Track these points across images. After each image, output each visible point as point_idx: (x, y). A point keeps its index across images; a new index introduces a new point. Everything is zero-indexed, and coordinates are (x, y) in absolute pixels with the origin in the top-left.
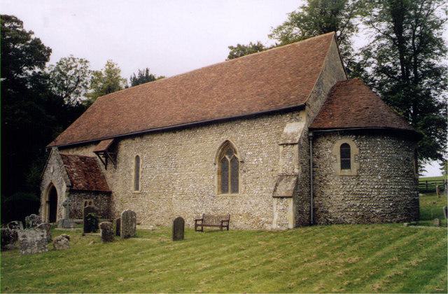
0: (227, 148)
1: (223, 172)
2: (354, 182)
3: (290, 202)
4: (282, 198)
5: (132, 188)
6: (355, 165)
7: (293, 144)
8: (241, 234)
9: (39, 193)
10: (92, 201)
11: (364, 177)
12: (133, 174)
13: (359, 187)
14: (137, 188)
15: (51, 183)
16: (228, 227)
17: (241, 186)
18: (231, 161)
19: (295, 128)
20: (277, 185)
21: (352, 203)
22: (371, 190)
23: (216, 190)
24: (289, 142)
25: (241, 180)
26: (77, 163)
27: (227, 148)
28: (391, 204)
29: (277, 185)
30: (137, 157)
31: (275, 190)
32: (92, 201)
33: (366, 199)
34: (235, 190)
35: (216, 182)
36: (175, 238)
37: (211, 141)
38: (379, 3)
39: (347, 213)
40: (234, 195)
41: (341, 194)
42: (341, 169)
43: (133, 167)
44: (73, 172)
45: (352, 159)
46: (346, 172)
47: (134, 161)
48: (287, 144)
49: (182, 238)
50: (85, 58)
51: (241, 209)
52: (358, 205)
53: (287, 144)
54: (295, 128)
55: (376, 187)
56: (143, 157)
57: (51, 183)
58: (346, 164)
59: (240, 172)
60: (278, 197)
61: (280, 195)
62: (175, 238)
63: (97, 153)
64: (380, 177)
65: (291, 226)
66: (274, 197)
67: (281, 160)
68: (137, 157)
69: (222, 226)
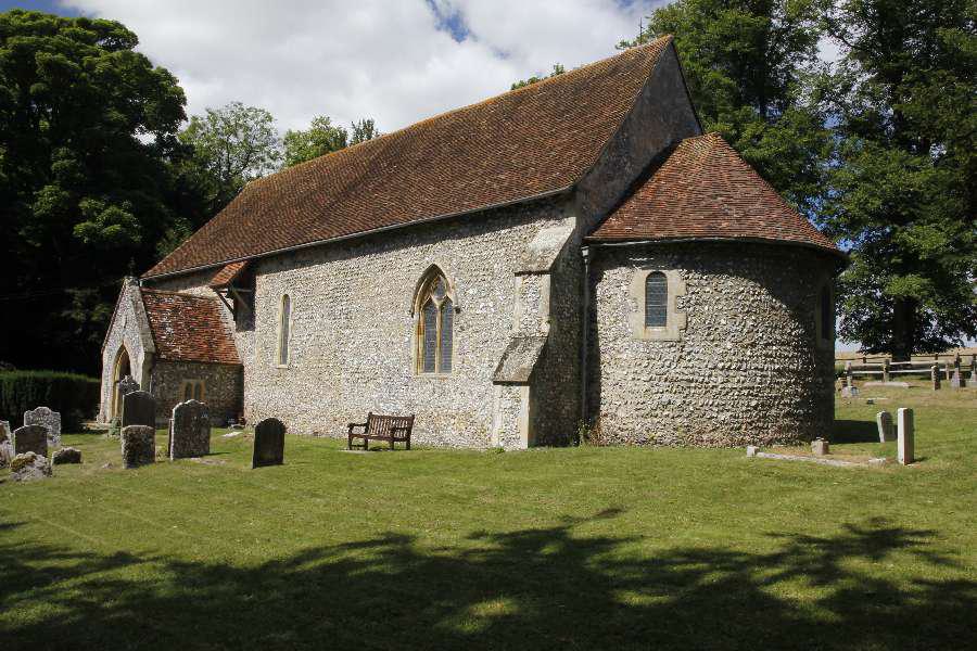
0: (433, 275)
1: (425, 329)
2: (672, 354)
3: (525, 392)
4: (510, 384)
5: (277, 359)
6: (675, 319)
7: (540, 273)
8: (325, 455)
9: (96, 369)
10: (202, 382)
11: (696, 344)
12: (278, 330)
13: (684, 363)
14: (284, 360)
15: (123, 347)
16: (407, 439)
17: (456, 361)
18: (442, 307)
19: (552, 236)
20: (504, 357)
21: (666, 397)
22: (708, 372)
23: (413, 364)
24: (534, 267)
25: (455, 347)
26: (175, 310)
27: (433, 275)
28: (754, 403)
29: (504, 357)
30: (286, 296)
31: (499, 369)
32: (202, 382)
33: (698, 391)
34: (446, 367)
35: (413, 348)
36: (259, 461)
37: (409, 263)
38: (740, 4)
39: (656, 420)
40: (444, 375)
41: (645, 378)
42: (646, 325)
43: (278, 318)
44: (163, 327)
45: (670, 304)
46: (657, 330)
47: (280, 306)
48: (530, 273)
49: (278, 461)
50: (240, 101)
51: (455, 406)
52: (679, 402)
53: (530, 273)
54: (552, 236)
55: (720, 365)
56: (296, 298)
57: (123, 347)
58: (656, 315)
59: (456, 328)
60: (502, 383)
61: (506, 379)
62: (259, 461)
63: (216, 288)
64: (729, 345)
65: (523, 444)
66: (496, 383)
67: (517, 305)
68: (286, 296)
69: (393, 439)
